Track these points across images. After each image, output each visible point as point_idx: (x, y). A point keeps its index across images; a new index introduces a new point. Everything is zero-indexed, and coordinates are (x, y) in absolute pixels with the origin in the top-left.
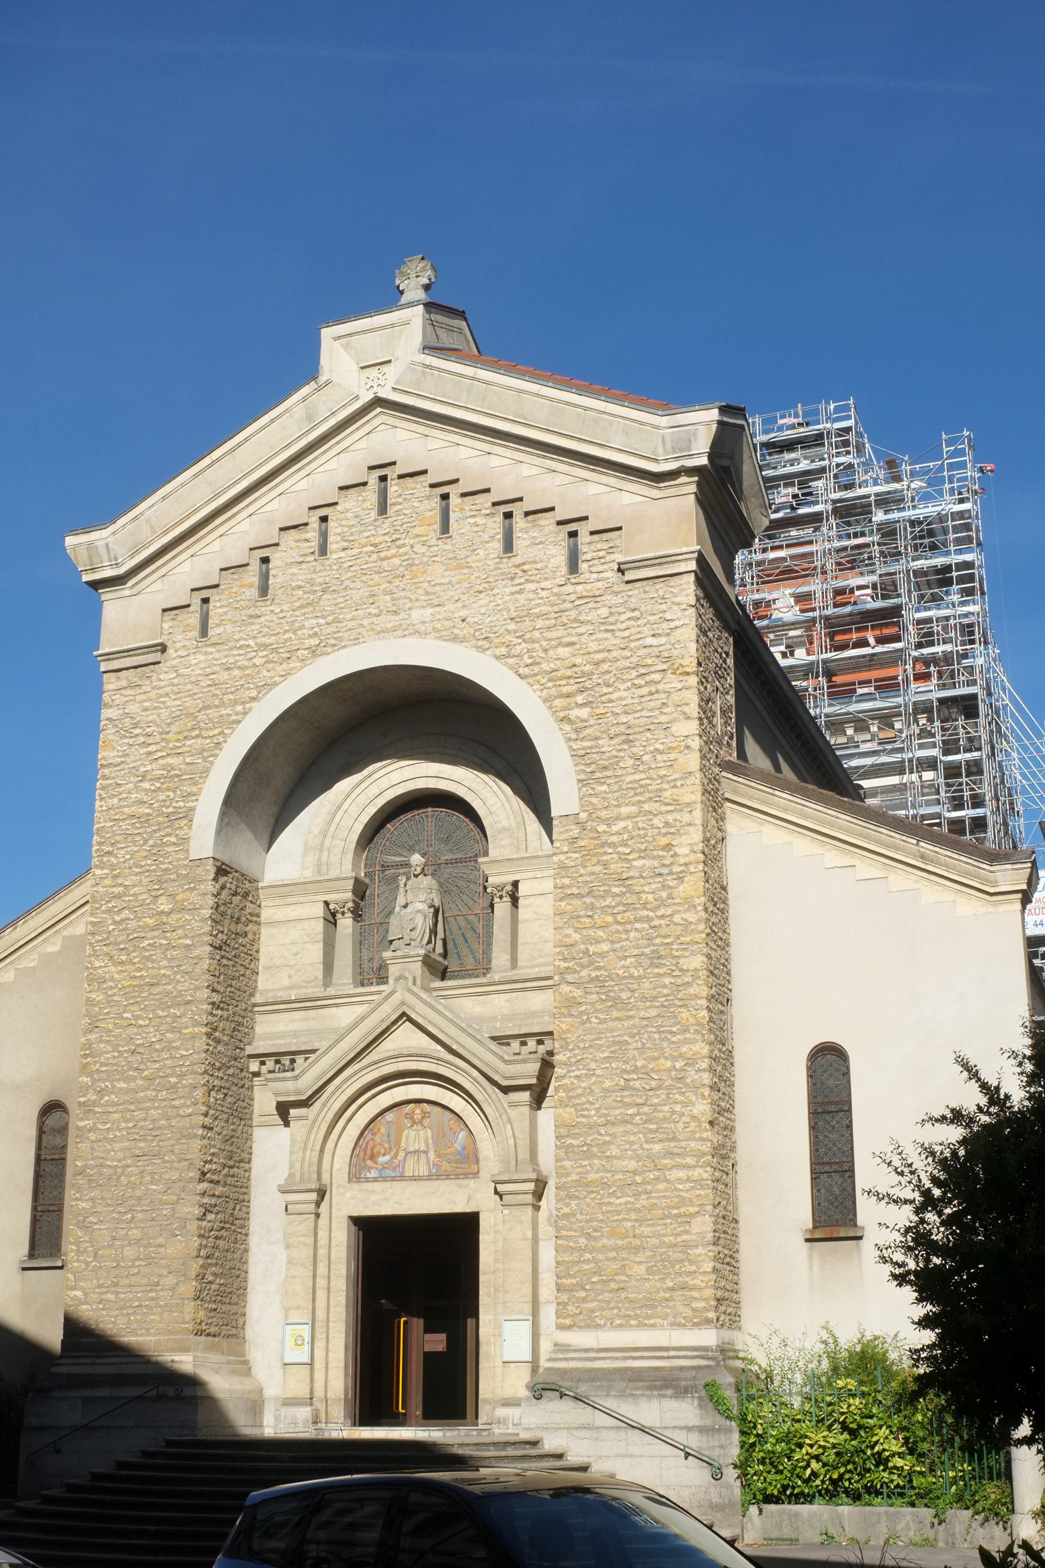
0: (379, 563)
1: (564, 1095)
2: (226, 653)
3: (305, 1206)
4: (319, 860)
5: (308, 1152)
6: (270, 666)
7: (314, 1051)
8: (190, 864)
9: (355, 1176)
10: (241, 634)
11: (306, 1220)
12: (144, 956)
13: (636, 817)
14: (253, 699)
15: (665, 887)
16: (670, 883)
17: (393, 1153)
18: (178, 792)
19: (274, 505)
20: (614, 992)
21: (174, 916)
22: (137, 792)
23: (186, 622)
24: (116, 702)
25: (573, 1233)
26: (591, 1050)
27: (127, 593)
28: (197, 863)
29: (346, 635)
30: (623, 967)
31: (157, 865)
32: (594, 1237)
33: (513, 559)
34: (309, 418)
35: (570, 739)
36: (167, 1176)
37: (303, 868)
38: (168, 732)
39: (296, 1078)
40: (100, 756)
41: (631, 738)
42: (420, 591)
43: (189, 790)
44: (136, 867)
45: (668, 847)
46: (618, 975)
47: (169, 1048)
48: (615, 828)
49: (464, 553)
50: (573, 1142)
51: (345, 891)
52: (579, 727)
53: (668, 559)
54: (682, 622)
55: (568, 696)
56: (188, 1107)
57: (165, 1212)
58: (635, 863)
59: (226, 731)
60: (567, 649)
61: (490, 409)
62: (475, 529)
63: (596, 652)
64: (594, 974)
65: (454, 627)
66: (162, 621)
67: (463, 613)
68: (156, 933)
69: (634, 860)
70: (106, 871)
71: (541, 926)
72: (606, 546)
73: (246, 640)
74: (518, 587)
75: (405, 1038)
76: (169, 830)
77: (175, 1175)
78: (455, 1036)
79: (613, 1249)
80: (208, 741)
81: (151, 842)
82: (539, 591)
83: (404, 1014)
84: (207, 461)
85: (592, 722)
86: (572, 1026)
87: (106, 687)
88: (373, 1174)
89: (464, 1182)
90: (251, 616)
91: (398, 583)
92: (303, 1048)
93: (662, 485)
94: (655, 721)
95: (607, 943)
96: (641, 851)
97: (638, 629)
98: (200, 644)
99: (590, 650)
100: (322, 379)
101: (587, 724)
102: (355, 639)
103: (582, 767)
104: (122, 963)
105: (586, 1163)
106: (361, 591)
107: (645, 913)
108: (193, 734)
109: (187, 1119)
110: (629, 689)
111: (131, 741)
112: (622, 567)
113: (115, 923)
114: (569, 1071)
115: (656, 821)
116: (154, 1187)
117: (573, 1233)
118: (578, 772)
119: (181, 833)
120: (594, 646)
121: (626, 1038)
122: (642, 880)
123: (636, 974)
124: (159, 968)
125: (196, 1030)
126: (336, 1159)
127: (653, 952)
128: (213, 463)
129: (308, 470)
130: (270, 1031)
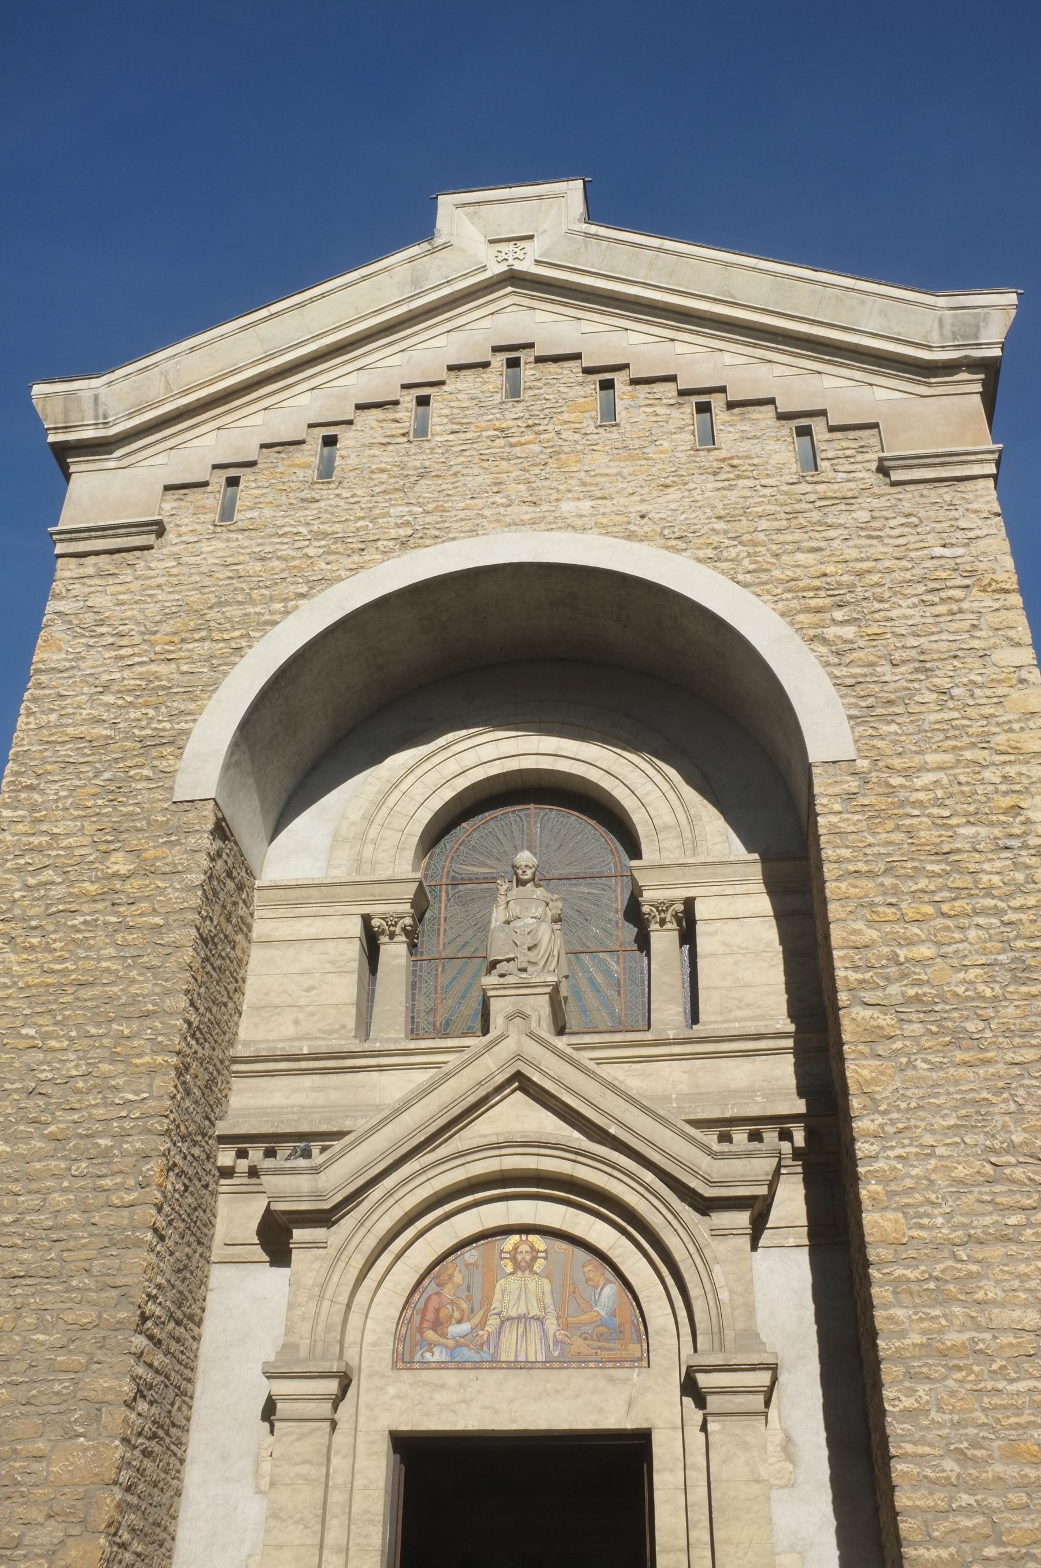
0: (508, 449)
1: (879, 1188)
2: (260, 541)
3: (311, 1405)
4: (360, 854)
5: (326, 1304)
6: (331, 558)
7: (340, 1135)
8: (174, 807)
9: (404, 1359)
10: (287, 520)
11: (313, 1431)
12: (74, 940)
13: (951, 768)
14: (302, 596)
15: (1016, 866)
16: (1027, 860)
17: (476, 1320)
18: (163, 710)
19: (351, 379)
20: (953, 1020)
21: (136, 882)
22: (91, 708)
23: (200, 503)
24: (73, 593)
25: (927, 1450)
26: (922, 1114)
27: (112, 464)
28: (186, 806)
29: (456, 525)
30: (964, 981)
31: (115, 808)
32: (973, 1459)
33: (715, 452)
34: (415, 282)
35: (828, 664)
36: (70, 1317)
37: (329, 865)
38: (155, 633)
39: (316, 1170)
40: (35, 659)
41: (928, 665)
42: (573, 482)
43: (182, 707)
44: (77, 808)
45: (1016, 810)
46: (956, 995)
47: (104, 1087)
48: (918, 783)
49: (637, 443)
50: (908, 1272)
51: (400, 901)
52: (841, 652)
53: (956, 459)
54: (985, 532)
55: (818, 611)
56: (129, 1190)
57: (57, 1387)
58: (961, 831)
59: (252, 634)
60: (811, 556)
61: (681, 286)
62: (654, 419)
63: (857, 560)
64: (911, 992)
65: (629, 523)
66: (162, 500)
67: (643, 508)
68: (100, 906)
69: (958, 826)
70: (21, 813)
71: (736, 963)
72: (855, 445)
73: (294, 526)
74: (727, 483)
76: (142, 760)
77: (88, 1315)
78: (617, 1113)
79: (1018, 1487)
80: (221, 645)
81: (107, 775)
82: (759, 488)
83: (518, 1076)
84: (263, 313)
85: (861, 643)
86: (882, 1073)
87: (59, 574)
88: (439, 1355)
89: (621, 1373)
90: (303, 500)
91: (537, 471)
92: (323, 1128)
93: (933, 380)
94: (964, 646)
95: (927, 945)
96: (968, 814)
97: (918, 538)
98: (219, 529)
99: (848, 557)
100: (439, 241)
101: (855, 646)
102: (471, 531)
103: (853, 700)
104: (32, 948)
105: (937, 1312)
106: (480, 478)
107: (989, 902)
108: (197, 636)
109: (125, 1213)
110: (915, 606)
111: (91, 642)
112: (887, 464)
113: (27, 887)
114: (884, 1148)
115: (987, 774)
116: (41, 1337)
117: (927, 1450)
118: (848, 706)
119: (163, 765)
120: (854, 554)
121: (985, 1094)
122: (977, 855)
123: (988, 993)
124: (99, 959)
125: (159, 1059)
126: (370, 1325)
127: (1014, 960)
128: (271, 317)
129: (403, 345)
130: (253, 1103)
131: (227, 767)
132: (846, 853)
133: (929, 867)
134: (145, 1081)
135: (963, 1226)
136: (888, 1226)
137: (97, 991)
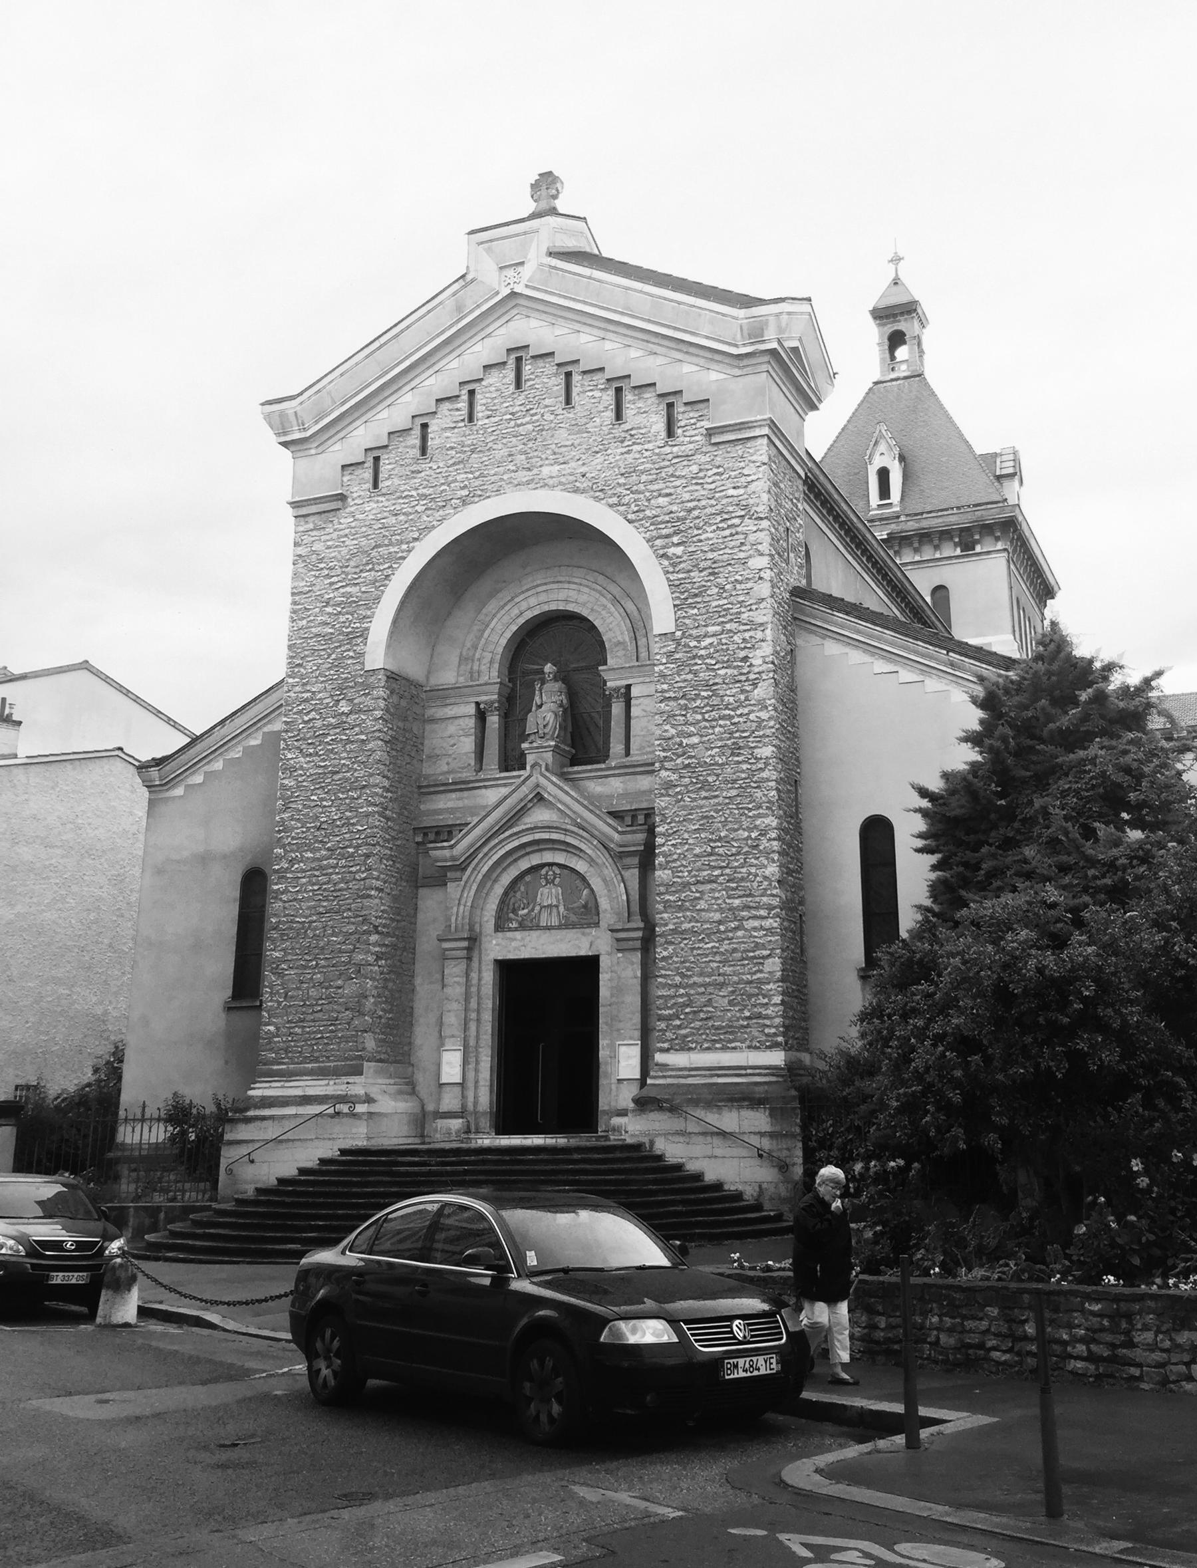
5: (462, 907)
6: (429, 512)
14: (416, 539)
15: (743, 691)
21: (353, 717)
29: (490, 487)
35: (668, 572)
39: (452, 847)
48: (703, 644)
49: (584, 420)
64: (687, 762)
75: (541, 816)
81: (333, 656)
88: (514, 925)
89: (587, 930)
96: (724, 662)
104: (311, 754)
107: (727, 712)
120: (687, 496)
127: (734, 744)
131: (388, 646)
132: (665, 687)
133: (703, 693)
134: (365, 820)
135: (695, 876)
136: (665, 877)
137: (340, 776)
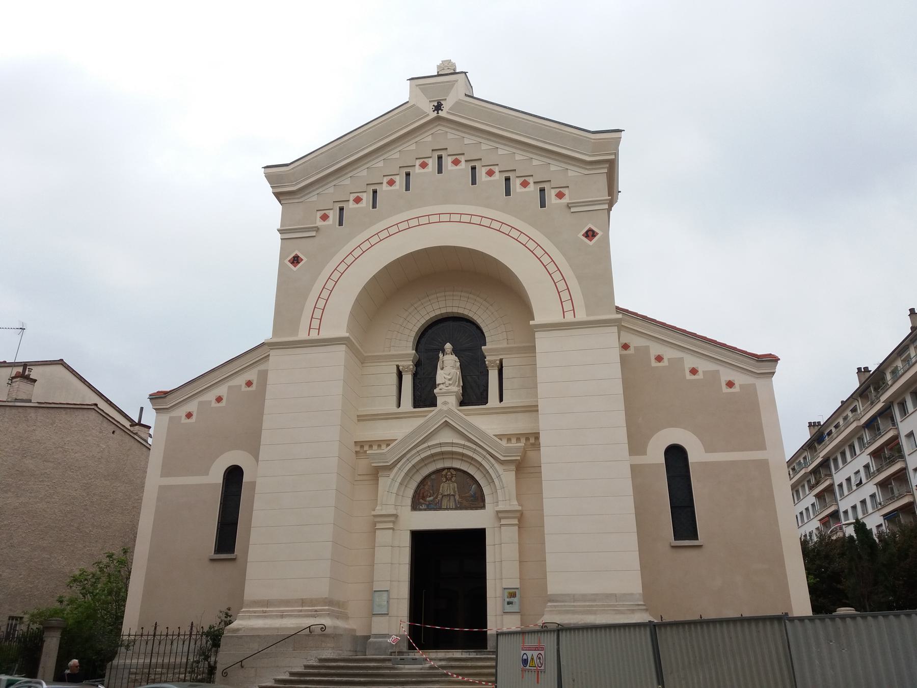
83: (446, 424)
88: (424, 507)
